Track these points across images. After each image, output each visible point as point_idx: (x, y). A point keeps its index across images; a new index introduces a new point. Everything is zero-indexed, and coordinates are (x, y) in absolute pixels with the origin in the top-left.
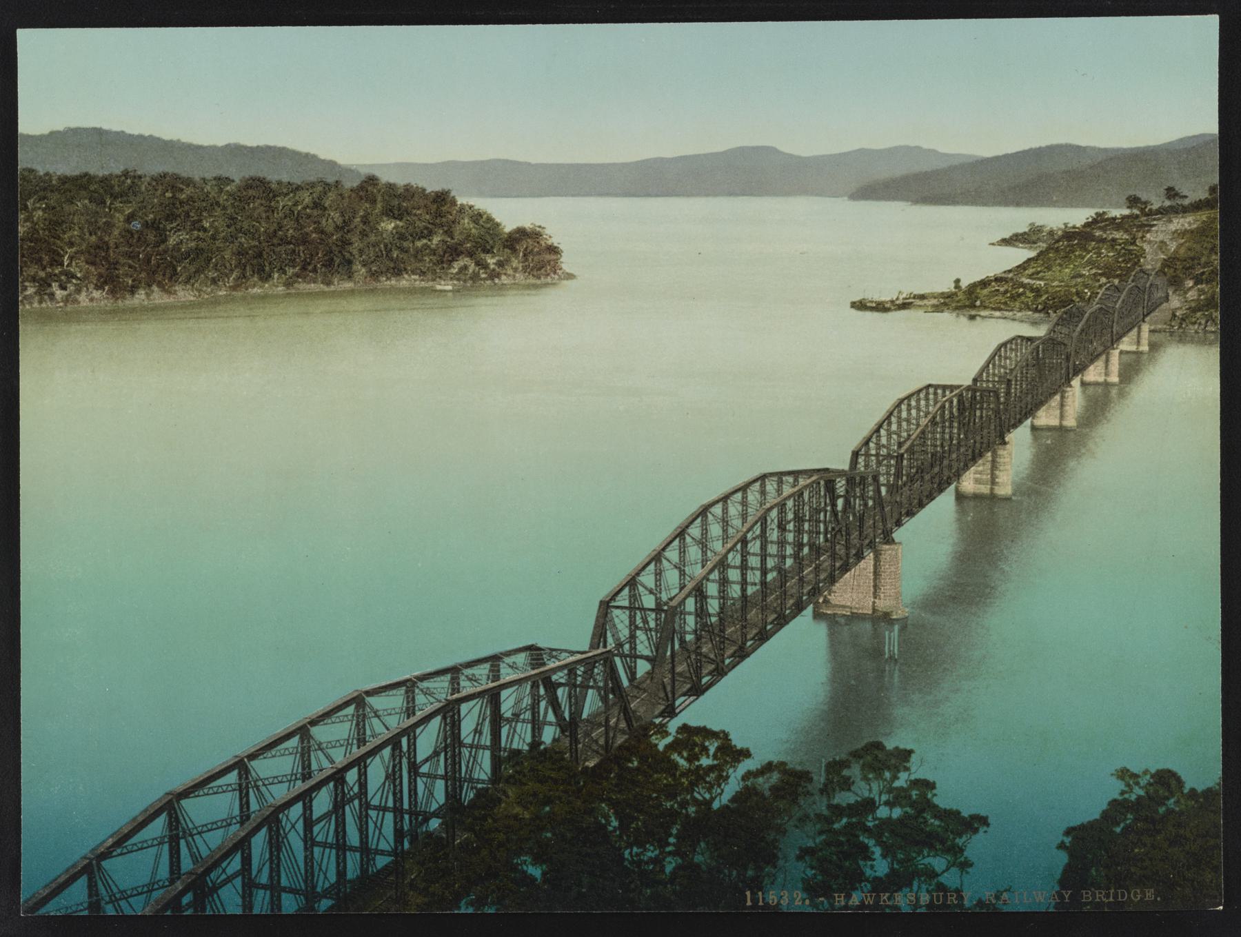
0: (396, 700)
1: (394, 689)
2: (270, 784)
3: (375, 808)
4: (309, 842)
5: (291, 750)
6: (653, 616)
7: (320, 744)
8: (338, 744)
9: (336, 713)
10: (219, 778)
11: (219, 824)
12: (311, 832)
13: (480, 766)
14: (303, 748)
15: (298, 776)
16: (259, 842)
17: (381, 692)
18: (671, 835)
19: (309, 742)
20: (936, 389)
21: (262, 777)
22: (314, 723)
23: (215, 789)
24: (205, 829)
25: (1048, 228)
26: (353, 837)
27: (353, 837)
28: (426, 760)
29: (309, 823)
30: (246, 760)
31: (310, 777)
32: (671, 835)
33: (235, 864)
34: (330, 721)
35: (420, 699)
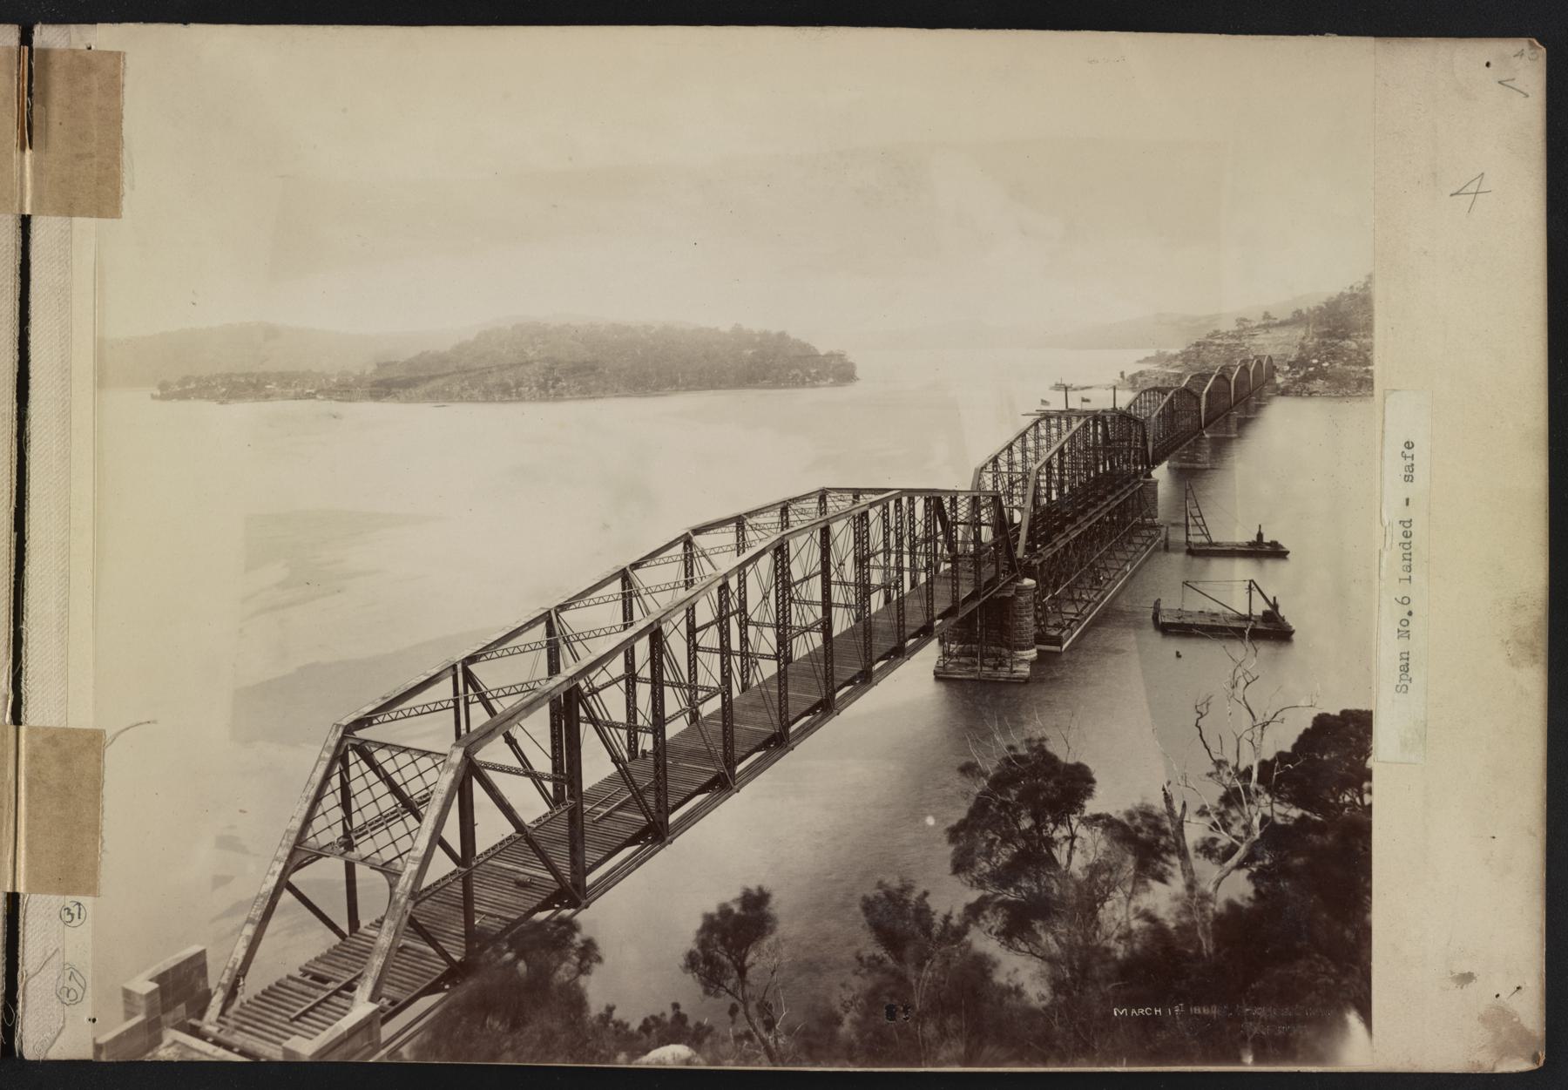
0: (728, 536)
1: (723, 526)
2: (586, 639)
3: (754, 624)
4: (693, 649)
5: (615, 597)
6: (983, 519)
7: (703, 551)
8: (677, 585)
9: (659, 554)
10: (666, 551)
11: (519, 688)
12: (694, 639)
13: (645, 718)
14: (686, 555)
15: (681, 583)
16: (642, 648)
17: (710, 530)
18: (519, 957)
19: (691, 550)
20: (1059, 418)
21: (489, 688)
22: (697, 531)
23: (666, 560)
24: (501, 693)
25: (1214, 860)
26: (735, 645)
27: (735, 645)
28: (815, 575)
29: (692, 630)
30: (628, 569)
31: (693, 584)
32: (519, 957)
33: (617, 667)
34: (653, 563)
35: (750, 535)
